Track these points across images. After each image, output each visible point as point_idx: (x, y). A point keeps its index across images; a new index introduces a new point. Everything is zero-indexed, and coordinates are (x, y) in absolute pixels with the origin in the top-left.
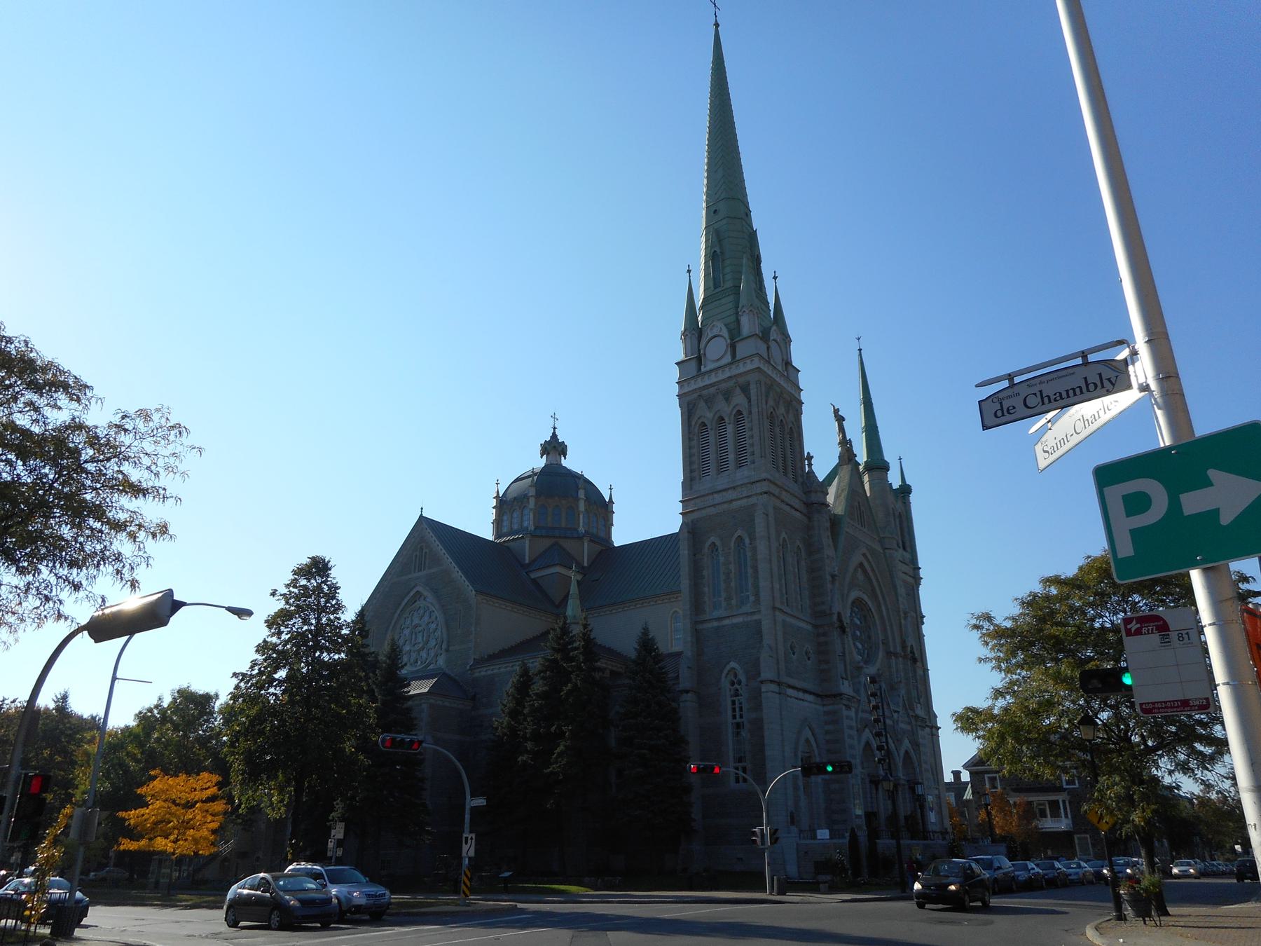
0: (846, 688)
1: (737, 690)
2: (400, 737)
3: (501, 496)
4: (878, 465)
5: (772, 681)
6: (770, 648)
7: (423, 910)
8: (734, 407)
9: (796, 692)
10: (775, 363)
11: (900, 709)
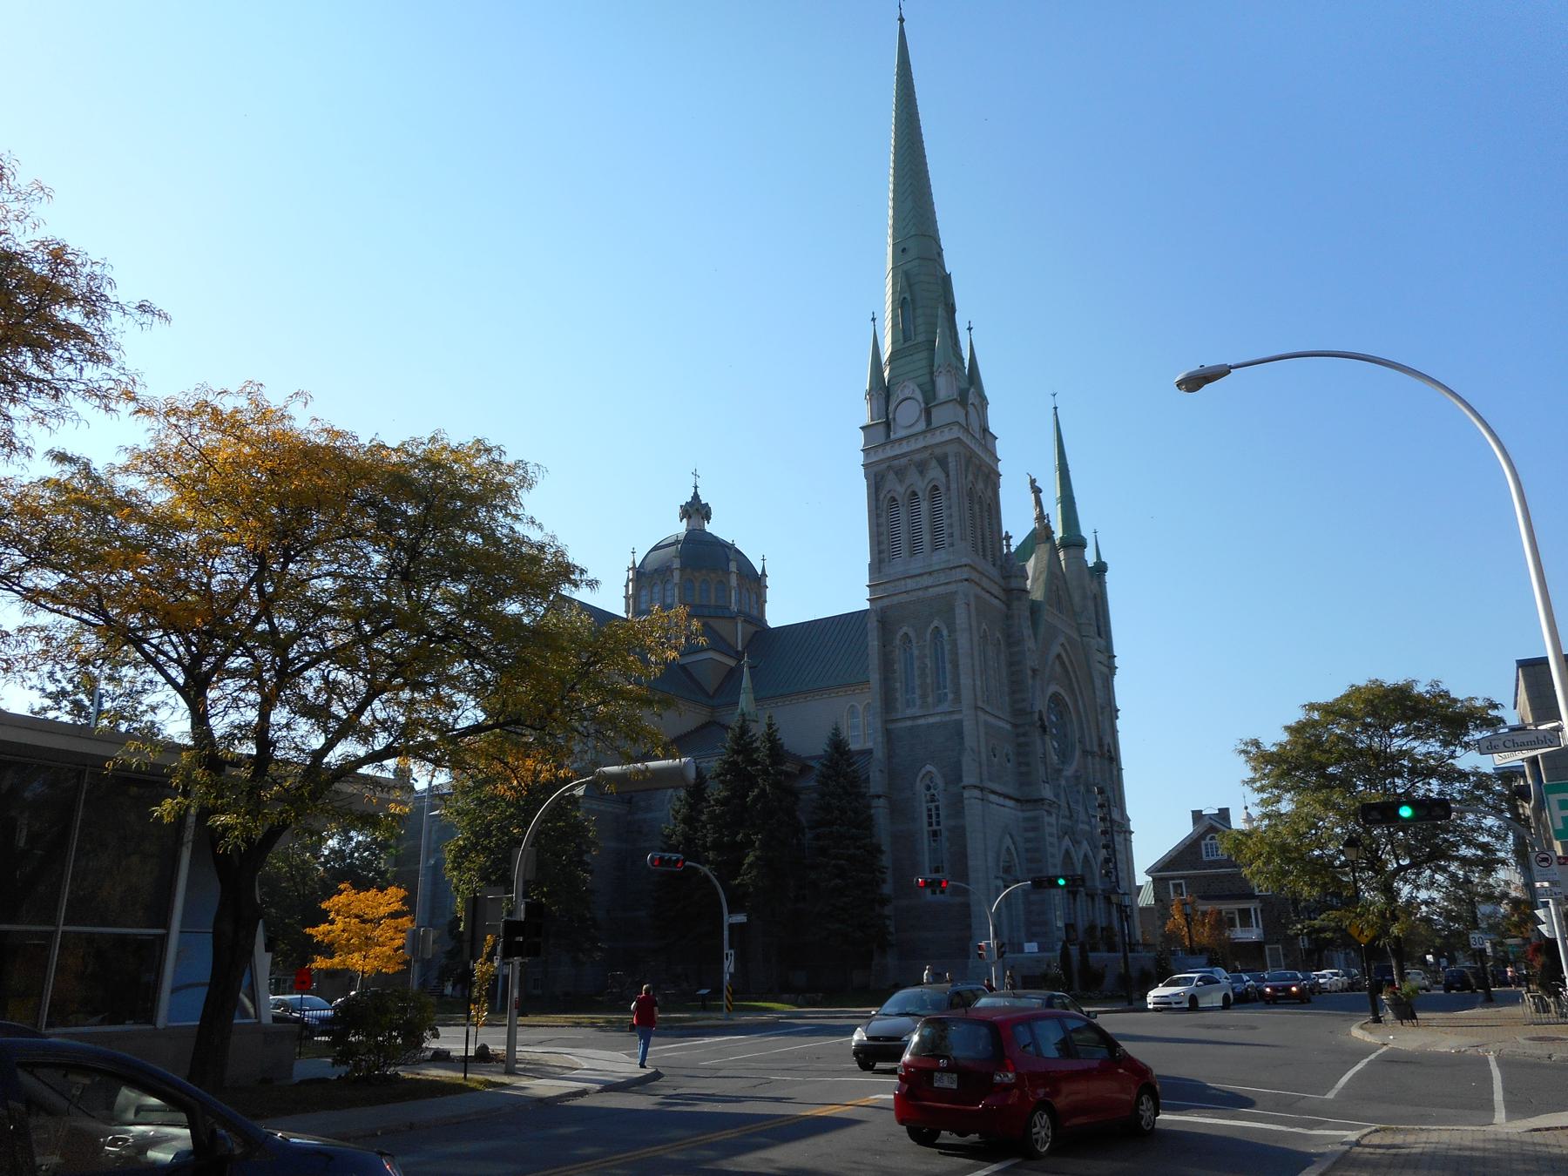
0: (1047, 792)
1: (934, 795)
3: (637, 566)
4: (1074, 542)
5: (975, 787)
6: (972, 750)
7: (696, 1023)
9: (1002, 799)
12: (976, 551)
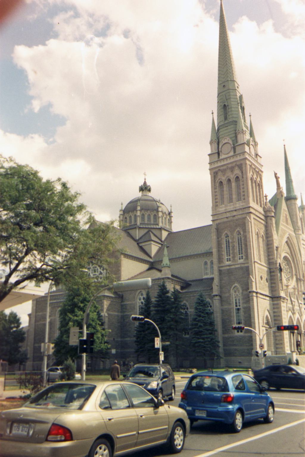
10: (252, 155)
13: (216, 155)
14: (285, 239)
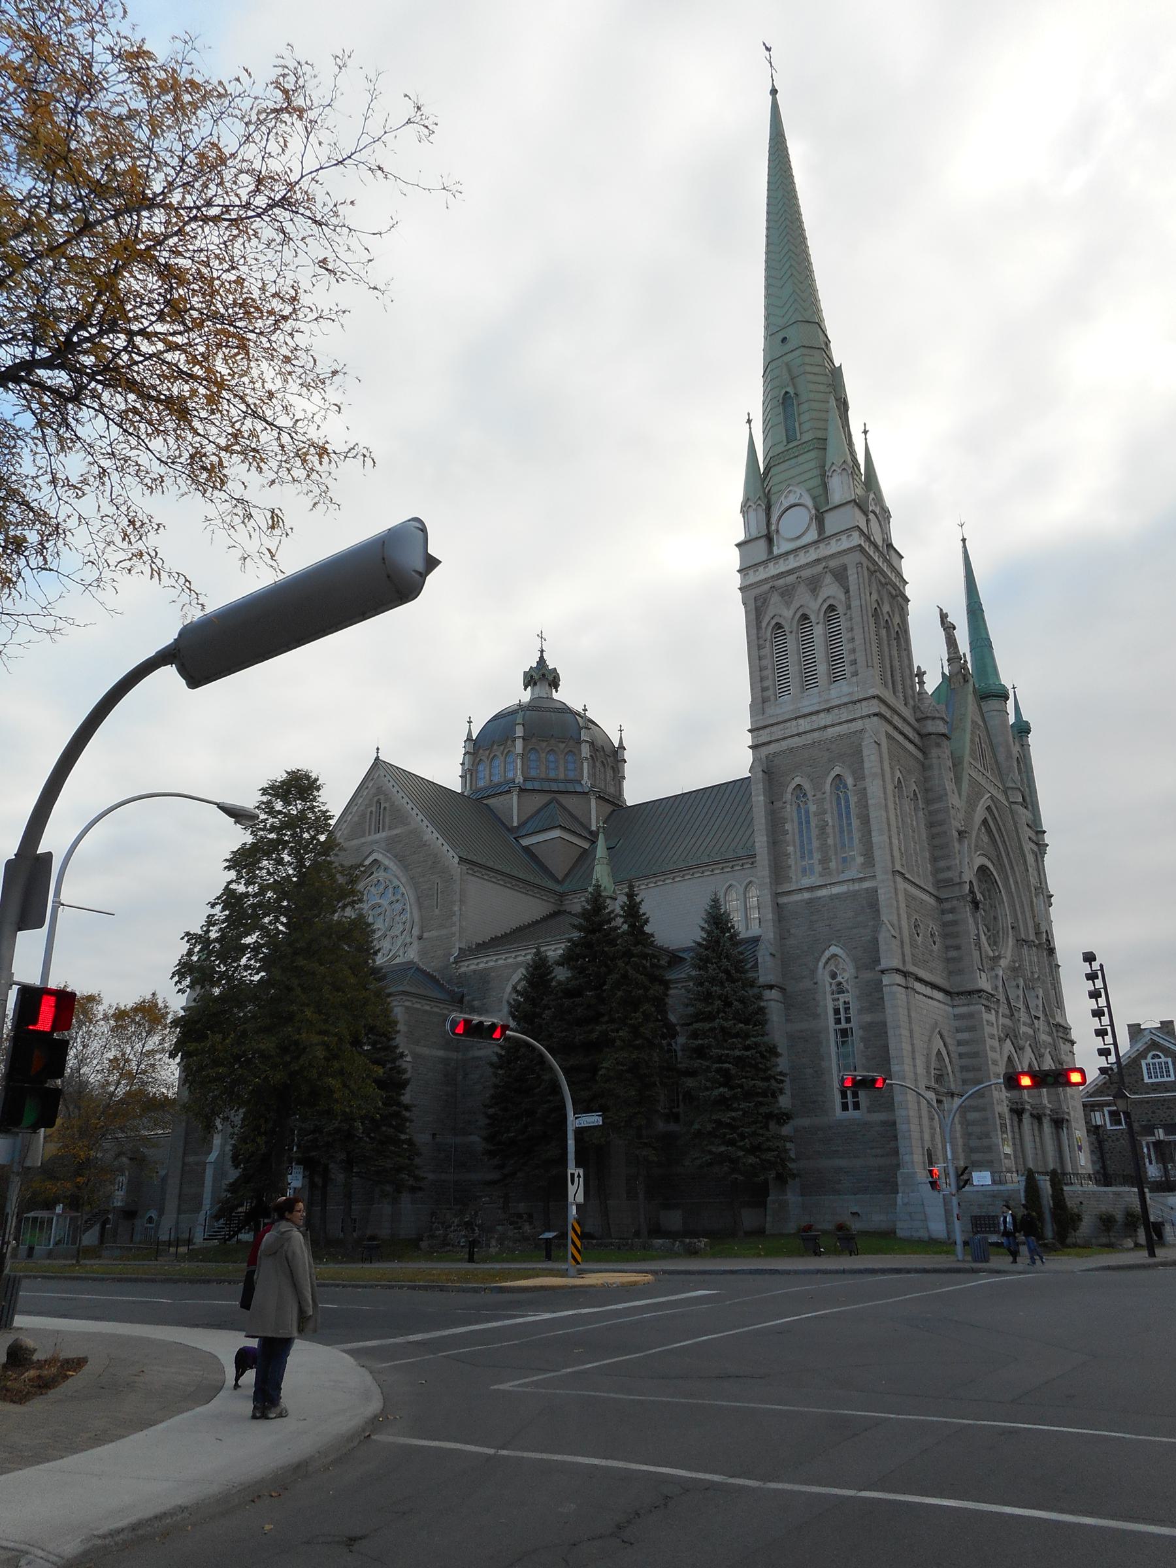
0: (984, 983)
2: (476, 1019)
8: (825, 601)
11: (1040, 1015)
12: (885, 685)
13: (762, 543)
14: (980, 813)
